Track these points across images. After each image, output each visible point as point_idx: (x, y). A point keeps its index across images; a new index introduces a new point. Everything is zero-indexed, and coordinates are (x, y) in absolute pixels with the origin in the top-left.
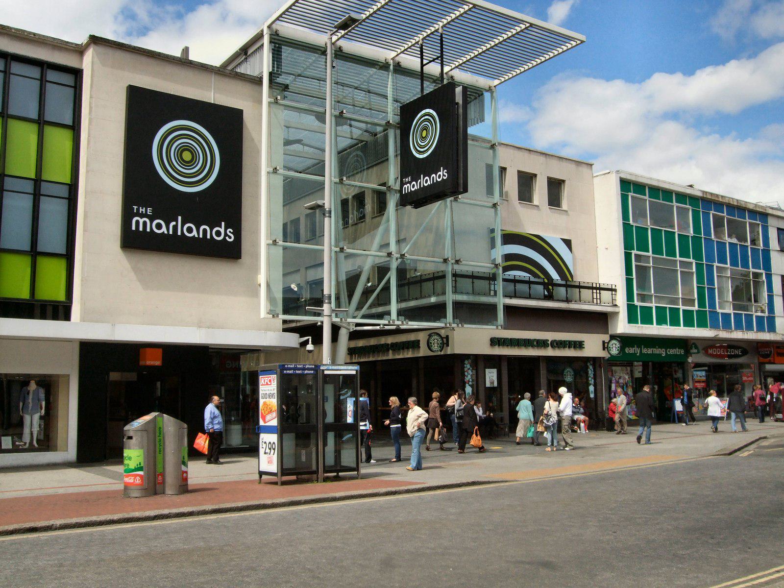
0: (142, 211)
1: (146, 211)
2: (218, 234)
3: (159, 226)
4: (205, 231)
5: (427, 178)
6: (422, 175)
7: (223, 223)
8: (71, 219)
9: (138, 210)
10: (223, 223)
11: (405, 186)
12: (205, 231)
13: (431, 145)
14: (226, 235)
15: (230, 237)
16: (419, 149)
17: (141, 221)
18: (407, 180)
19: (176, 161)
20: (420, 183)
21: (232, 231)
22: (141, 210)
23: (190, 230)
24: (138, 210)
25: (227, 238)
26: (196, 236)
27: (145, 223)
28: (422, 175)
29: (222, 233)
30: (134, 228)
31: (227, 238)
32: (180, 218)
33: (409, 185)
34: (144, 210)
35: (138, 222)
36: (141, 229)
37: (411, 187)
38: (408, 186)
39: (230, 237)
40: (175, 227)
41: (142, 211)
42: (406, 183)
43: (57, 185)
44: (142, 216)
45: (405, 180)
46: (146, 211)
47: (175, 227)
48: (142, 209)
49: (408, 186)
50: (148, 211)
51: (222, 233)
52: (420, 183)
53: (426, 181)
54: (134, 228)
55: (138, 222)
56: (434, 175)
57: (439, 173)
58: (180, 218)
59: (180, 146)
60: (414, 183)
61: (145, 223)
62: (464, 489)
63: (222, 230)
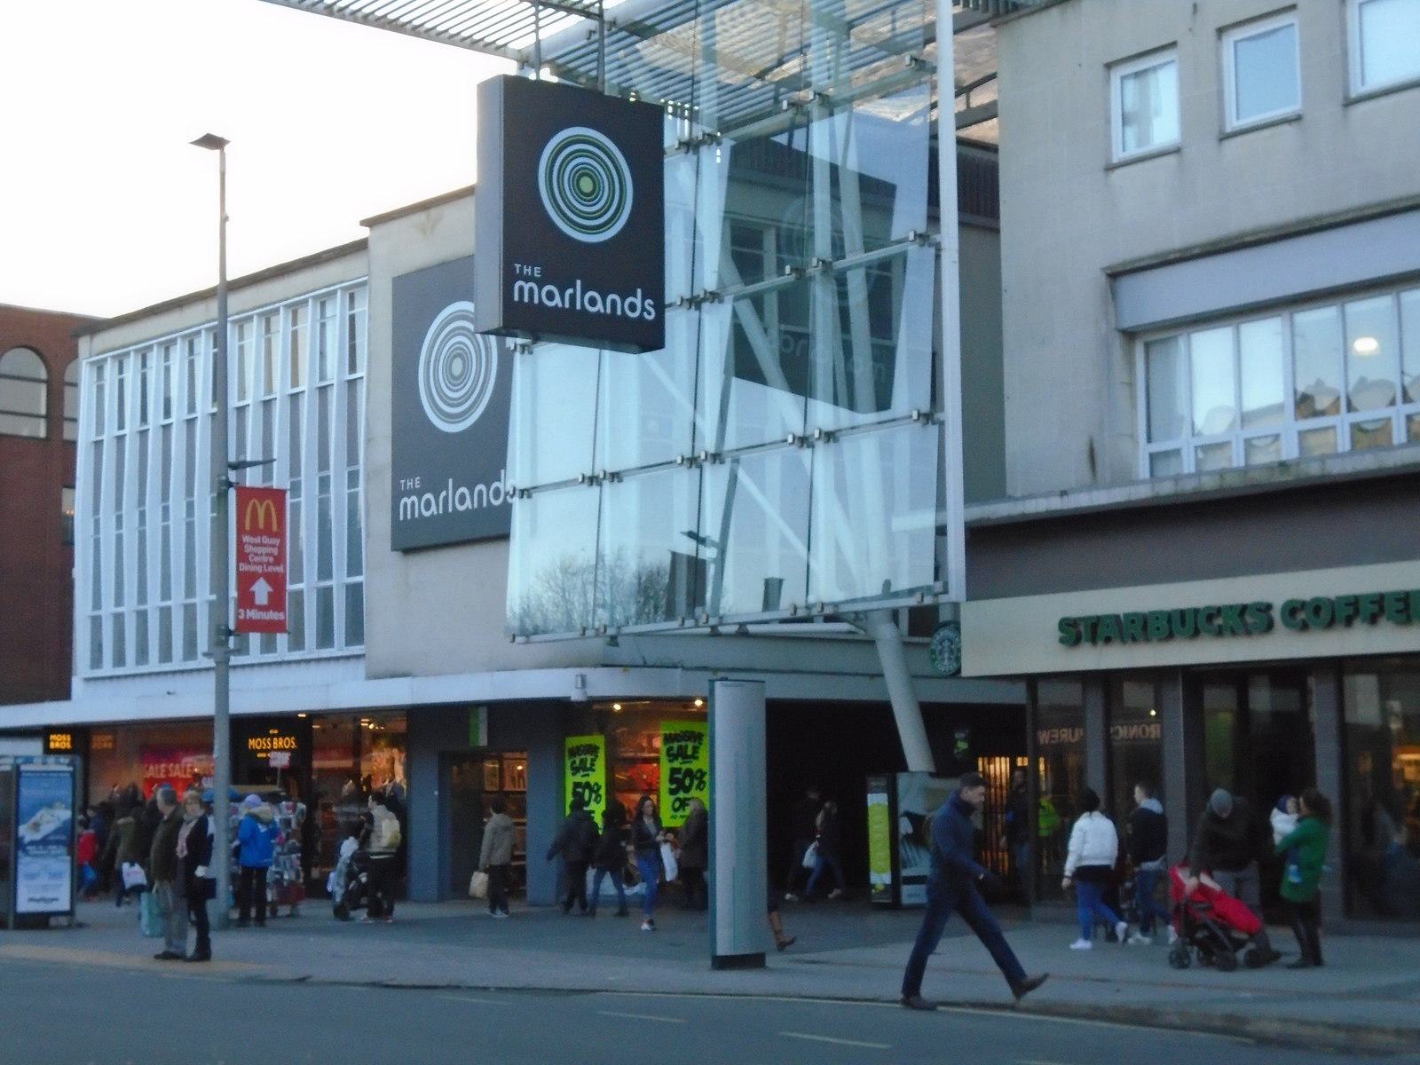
0: (527, 272)
1: (533, 271)
2: (633, 307)
3: (550, 296)
4: (614, 303)
5: (463, 490)
6: (450, 481)
7: (639, 291)
8: (219, 377)
9: (521, 269)
10: (639, 291)
11: (405, 500)
12: (614, 303)
13: (481, 390)
14: (643, 309)
15: (649, 314)
16: (451, 387)
17: (527, 286)
18: (410, 484)
19: (569, 184)
20: (446, 499)
21: (652, 303)
22: (525, 270)
23: (593, 302)
24: (521, 269)
25: (645, 314)
26: (602, 311)
27: (531, 291)
28: (450, 481)
29: (637, 306)
30: (516, 298)
31: (645, 314)
32: (579, 282)
33: (414, 498)
34: (529, 270)
35: (521, 289)
36: (526, 299)
37: (424, 506)
38: (413, 503)
39: (649, 314)
40: (573, 297)
41: (527, 272)
42: (409, 493)
43: (12, 410)
44: (527, 279)
45: (405, 484)
46: (533, 271)
47: (573, 297)
48: (527, 268)
49: (413, 503)
50: (536, 272)
51: (637, 306)
52: (446, 499)
53: (462, 499)
54: (516, 298)
55: (521, 289)
56: (481, 487)
57: (496, 484)
58: (579, 282)
59: (617, 185)
60: (429, 496)
61: (531, 291)
62: (468, 999)
63: (638, 302)
